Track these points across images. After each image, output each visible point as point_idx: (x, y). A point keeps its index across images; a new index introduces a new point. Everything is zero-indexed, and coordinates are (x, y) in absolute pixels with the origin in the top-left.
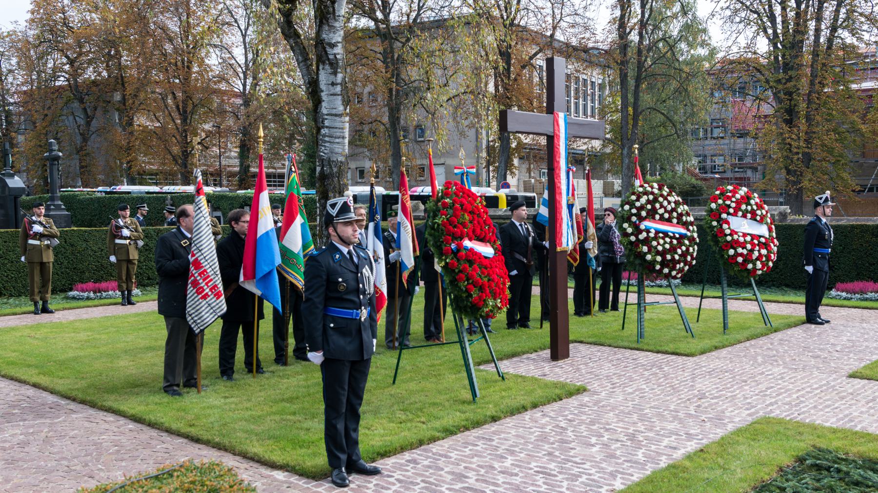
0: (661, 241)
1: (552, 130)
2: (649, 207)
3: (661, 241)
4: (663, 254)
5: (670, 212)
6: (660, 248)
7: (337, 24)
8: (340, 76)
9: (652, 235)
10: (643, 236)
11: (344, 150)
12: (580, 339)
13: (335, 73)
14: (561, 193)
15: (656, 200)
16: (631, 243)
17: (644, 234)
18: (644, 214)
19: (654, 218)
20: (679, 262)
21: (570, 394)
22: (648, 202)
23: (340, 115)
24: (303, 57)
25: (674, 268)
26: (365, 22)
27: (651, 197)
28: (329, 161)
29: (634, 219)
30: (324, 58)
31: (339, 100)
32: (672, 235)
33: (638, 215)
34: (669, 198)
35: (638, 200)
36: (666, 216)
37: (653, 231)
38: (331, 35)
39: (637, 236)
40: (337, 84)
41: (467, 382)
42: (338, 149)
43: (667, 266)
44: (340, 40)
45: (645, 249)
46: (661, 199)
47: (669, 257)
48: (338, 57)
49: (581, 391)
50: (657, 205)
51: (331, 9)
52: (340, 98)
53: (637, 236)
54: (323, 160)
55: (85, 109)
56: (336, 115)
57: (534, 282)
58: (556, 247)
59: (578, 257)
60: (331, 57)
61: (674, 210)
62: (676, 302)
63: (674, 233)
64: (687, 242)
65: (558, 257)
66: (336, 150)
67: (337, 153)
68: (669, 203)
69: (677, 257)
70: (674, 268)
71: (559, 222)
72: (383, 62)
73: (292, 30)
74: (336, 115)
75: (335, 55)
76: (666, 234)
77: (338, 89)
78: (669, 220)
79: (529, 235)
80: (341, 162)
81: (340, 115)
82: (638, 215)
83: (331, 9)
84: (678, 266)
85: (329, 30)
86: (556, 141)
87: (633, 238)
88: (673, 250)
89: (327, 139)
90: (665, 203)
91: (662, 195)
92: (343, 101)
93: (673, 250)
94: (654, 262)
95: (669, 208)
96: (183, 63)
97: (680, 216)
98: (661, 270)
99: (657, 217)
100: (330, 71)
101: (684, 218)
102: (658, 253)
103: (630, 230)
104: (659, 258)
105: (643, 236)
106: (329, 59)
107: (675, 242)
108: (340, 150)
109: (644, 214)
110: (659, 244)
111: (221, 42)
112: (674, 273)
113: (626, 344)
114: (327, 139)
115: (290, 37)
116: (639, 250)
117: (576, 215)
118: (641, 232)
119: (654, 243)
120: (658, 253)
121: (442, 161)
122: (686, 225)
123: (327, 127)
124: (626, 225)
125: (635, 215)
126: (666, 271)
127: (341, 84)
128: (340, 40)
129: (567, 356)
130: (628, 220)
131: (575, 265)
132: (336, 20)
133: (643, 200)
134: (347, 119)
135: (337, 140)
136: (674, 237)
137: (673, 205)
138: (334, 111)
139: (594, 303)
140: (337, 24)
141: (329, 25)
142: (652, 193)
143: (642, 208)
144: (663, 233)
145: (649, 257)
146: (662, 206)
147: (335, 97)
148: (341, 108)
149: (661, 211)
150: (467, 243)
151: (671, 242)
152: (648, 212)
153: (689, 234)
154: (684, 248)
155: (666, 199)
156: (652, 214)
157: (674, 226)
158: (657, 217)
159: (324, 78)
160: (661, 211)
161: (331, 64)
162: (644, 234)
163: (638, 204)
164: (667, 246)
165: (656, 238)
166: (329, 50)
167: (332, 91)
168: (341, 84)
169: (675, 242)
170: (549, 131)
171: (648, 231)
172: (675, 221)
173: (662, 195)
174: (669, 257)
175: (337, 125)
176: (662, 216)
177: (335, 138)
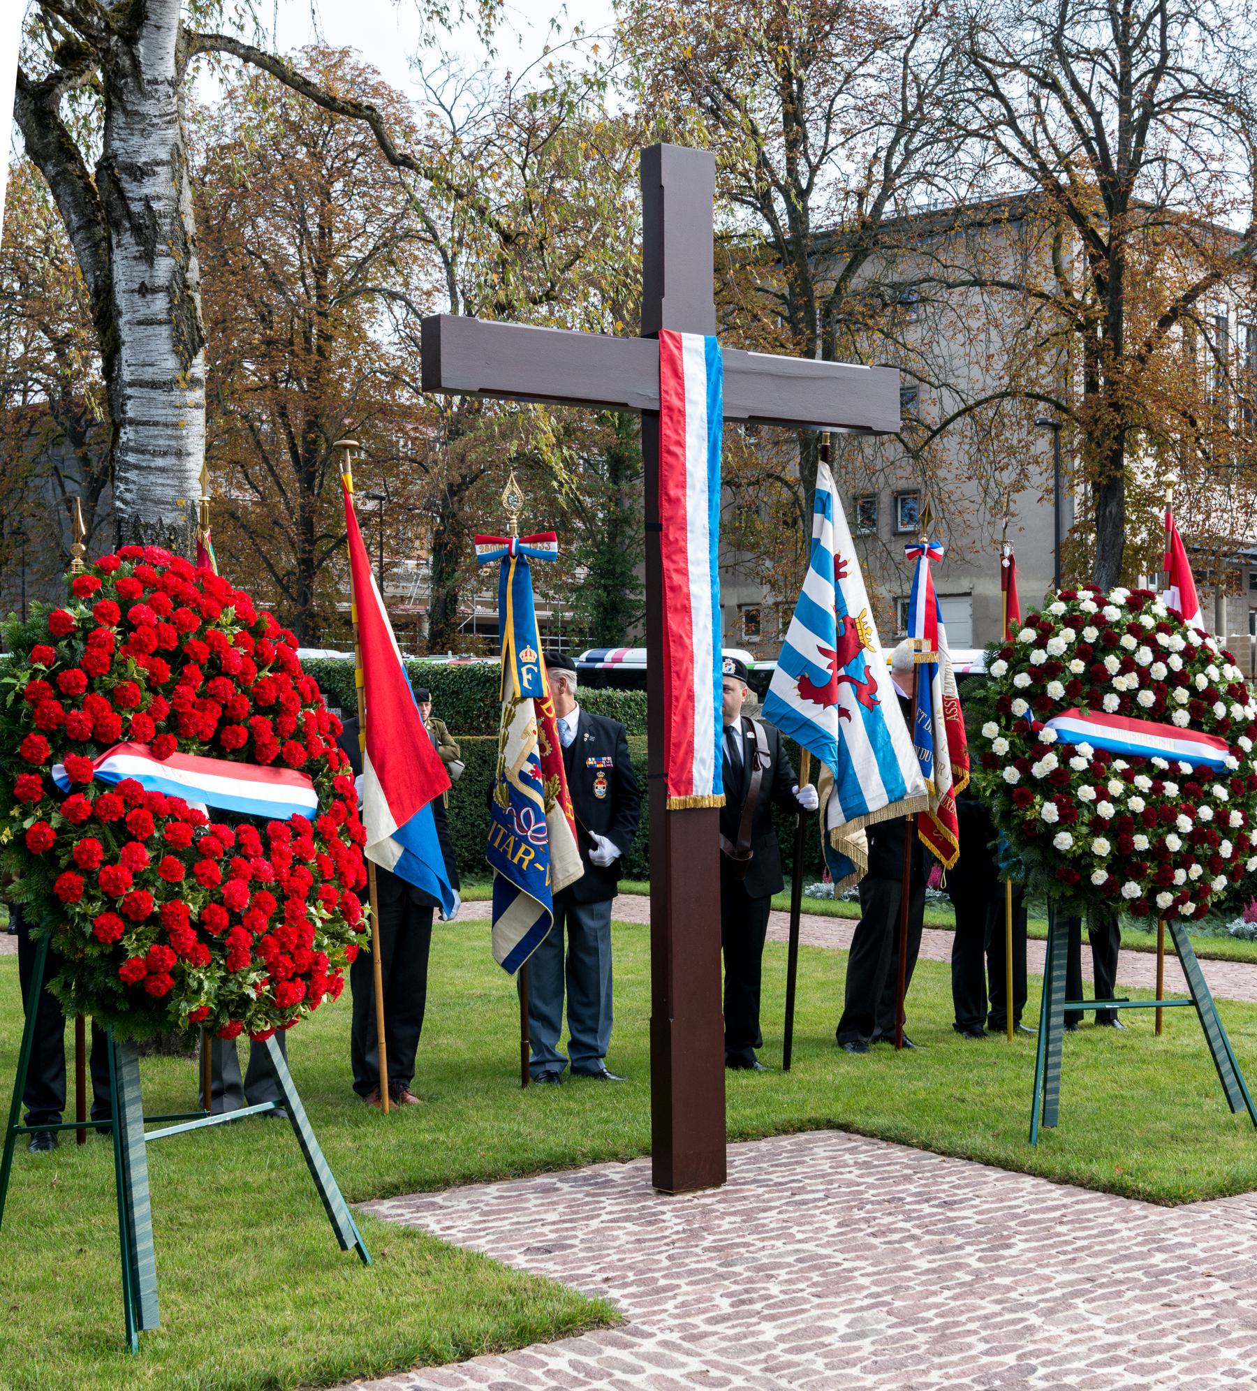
0: (1116, 787)
1: (652, 392)
2: (1078, 666)
3: (1116, 787)
4: (1120, 829)
5: (1163, 689)
6: (1106, 810)
7: (149, 108)
8: (164, 267)
9: (1079, 764)
10: (1047, 765)
11: (182, 491)
12: (842, 1119)
13: (148, 257)
14: (686, 610)
15: (1109, 642)
16: (1005, 788)
17: (1050, 761)
18: (1056, 689)
19: (1096, 705)
20: (1184, 860)
21: (564, 1329)
22: (1079, 649)
23: (167, 386)
24: (82, 215)
25: (1164, 882)
26: (743, 218)
27: (1091, 634)
28: (136, 522)
29: (1020, 707)
30: (118, 213)
31: (161, 340)
32: (1163, 764)
33: (1036, 696)
34: (1162, 639)
35: (1041, 643)
36: (1147, 698)
37: (1086, 750)
38: (136, 140)
39: (1025, 768)
40: (154, 291)
41: (114, 1273)
42: (163, 488)
43: (1137, 874)
45: (1050, 812)
46: (1129, 641)
47: (1142, 842)
48: (156, 206)
49: (599, 1318)
50: (1112, 663)
51: (126, 62)
52: (165, 331)
53: (1025, 768)
54: (119, 523)
55: (85, 461)
56: (153, 385)
57: (929, 916)
58: (666, 796)
59: (955, 841)
60: (136, 207)
61: (1175, 679)
62: (1194, 1003)
63: (1173, 761)
64: (1220, 792)
65: (676, 827)
66: (158, 492)
67: (158, 502)
68: (1161, 654)
69: (1174, 843)
70: (1164, 882)
71: (678, 708)
72: (788, 320)
73: (52, 137)
74: (153, 385)
75: (147, 200)
76: (1140, 761)
77: (160, 304)
78: (1160, 715)
79: (754, 765)
80: (172, 529)
81: (167, 386)
82: (1036, 696)
83: (126, 62)
84: (1180, 876)
85: (128, 126)
86: (667, 430)
87: (1011, 775)
88: (1159, 815)
89: (131, 458)
90: (1145, 656)
91: (1136, 630)
92: (177, 340)
93: (1159, 815)
94: (1084, 860)
95: (1159, 672)
96: (307, 340)
97: (1202, 702)
98: (1113, 887)
99: (1111, 702)
100: (135, 250)
101: (1220, 710)
102: (1099, 826)
103: (1001, 746)
104: (1102, 846)
105: (1047, 765)
106: (129, 215)
107: (1171, 789)
108: (170, 493)
109: (1056, 689)
110: (1103, 794)
111: (406, 284)
112: (1165, 900)
113: (978, 1141)
114: (131, 458)
115: (47, 158)
116: (1030, 815)
117: (946, 700)
118: (1040, 750)
119: (1087, 793)
120: (1099, 826)
121: (964, 586)
122: (1225, 732)
123: (132, 422)
124: (990, 729)
125: (1024, 693)
126: (1132, 890)
127: (168, 289)
128: (163, 155)
129: (714, 1175)
130: (1001, 710)
131: (950, 864)
132: (146, 96)
133: (1060, 643)
134: (198, 395)
135: (160, 462)
136: (1173, 773)
137: (1176, 663)
138: (148, 374)
139: (1021, 997)
140: (149, 108)
141: (127, 113)
142: (1098, 620)
143: (1053, 668)
144: (1127, 757)
145: (1064, 840)
146: (1128, 665)
147: (150, 330)
148: (171, 363)
149: (1128, 682)
150: (128, 764)
151: (1157, 789)
152: (1073, 687)
153: (1233, 763)
154: (1206, 813)
155: (1146, 638)
156: (1088, 692)
157: (1178, 734)
158: (1111, 702)
159: (124, 272)
160: (1128, 682)
161: (137, 230)
162: (1050, 761)
163: (1038, 657)
164: (1137, 804)
165: (1096, 775)
166: (132, 189)
167: (144, 312)
168: (168, 289)
169: (1171, 789)
170: (641, 394)
171: (1066, 750)
172: (1182, 717)
173: (1136, 630)
174: (1142, 842)
175: (159, 414)
176: (1128, 699)
177: (154, 454)
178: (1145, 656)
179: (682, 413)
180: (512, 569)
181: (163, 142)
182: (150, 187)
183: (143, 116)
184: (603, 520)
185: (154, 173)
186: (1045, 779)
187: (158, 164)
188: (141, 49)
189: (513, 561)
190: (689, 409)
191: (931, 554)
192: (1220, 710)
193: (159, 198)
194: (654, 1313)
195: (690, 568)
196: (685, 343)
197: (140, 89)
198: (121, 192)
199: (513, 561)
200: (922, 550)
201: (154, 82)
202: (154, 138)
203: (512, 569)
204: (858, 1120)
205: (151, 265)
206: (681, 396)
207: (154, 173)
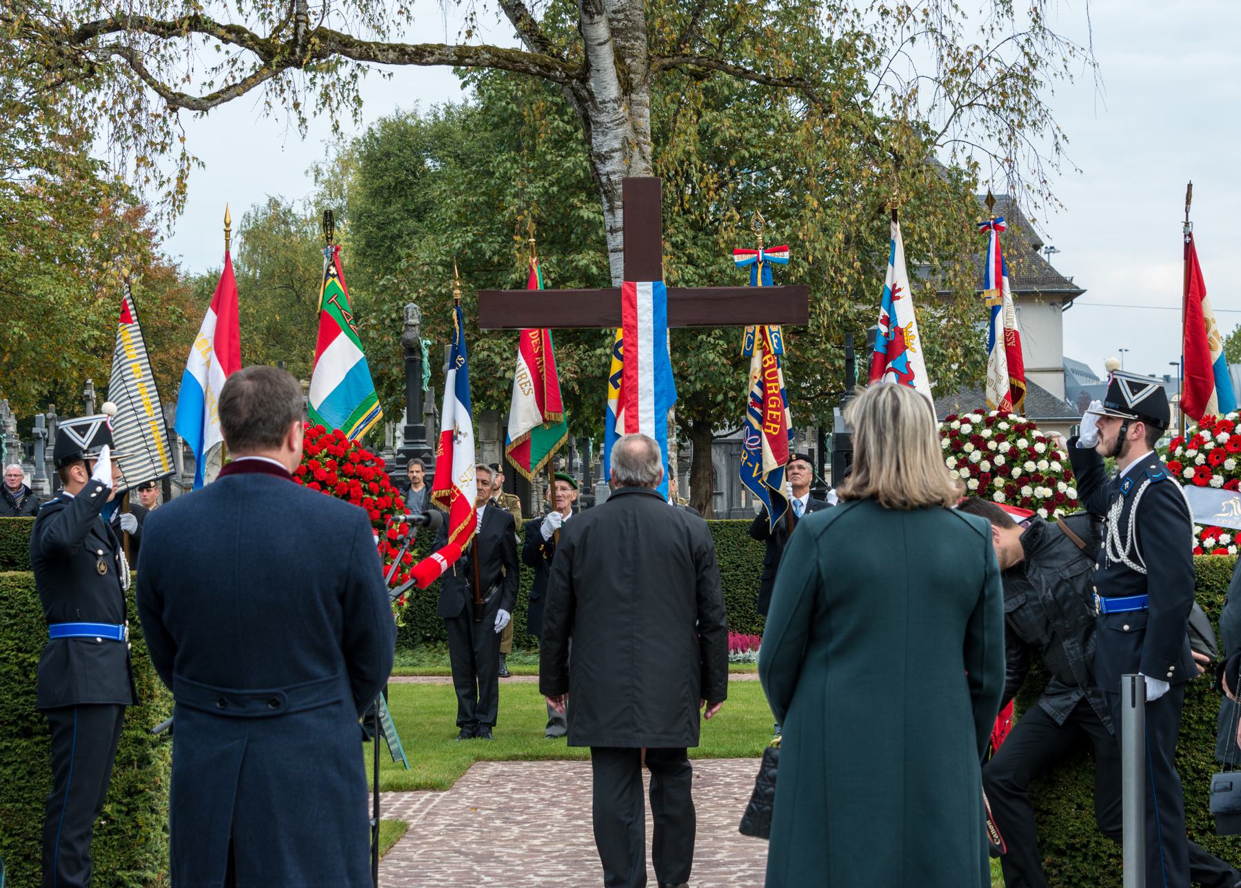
7: (603, 118)
44: (617, 145)
46: (969, 447)
48: (613, 178)
61: (995, 471)
75: (608, 174)
90: (976, 456)
95: (985, 466)
128: (617, 145)
132: (600, 111)
140: (603, 118)
178: (976, 456)
179: (635, 327)
180: (760, 271)
181: (616, 137)
182: (609, 167)
183: (601, 124)
184: (133, 637)
185: (612, 157)
186: (1120, 679)
187: (613, 151)
188: (592, 84)
189: (760, 266)
190: (640, 325)
191: (996, 227)
192: (1026, 491)
193: (614, 173)
194: (550, 876)
195: (640, 414)
196: (638, 288)
197: (596, 107)
198: (596, 169)
199: (760, 266)
200: (989, 226)
201: (604, 102)
202: (610, 135)
203: (760, 271)
204: (717, 751)
205: (613, 214)
206: (635, 318)
207: (612, 157)
